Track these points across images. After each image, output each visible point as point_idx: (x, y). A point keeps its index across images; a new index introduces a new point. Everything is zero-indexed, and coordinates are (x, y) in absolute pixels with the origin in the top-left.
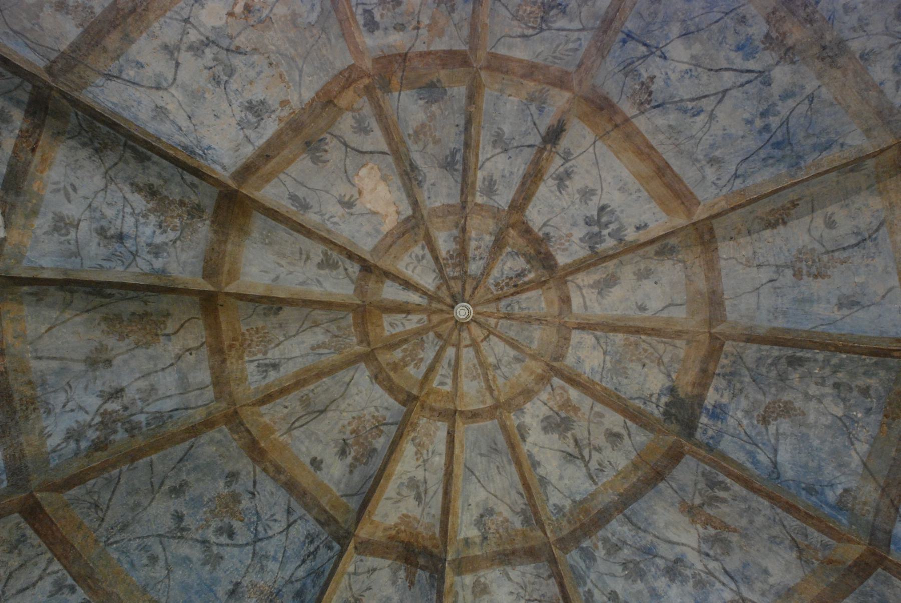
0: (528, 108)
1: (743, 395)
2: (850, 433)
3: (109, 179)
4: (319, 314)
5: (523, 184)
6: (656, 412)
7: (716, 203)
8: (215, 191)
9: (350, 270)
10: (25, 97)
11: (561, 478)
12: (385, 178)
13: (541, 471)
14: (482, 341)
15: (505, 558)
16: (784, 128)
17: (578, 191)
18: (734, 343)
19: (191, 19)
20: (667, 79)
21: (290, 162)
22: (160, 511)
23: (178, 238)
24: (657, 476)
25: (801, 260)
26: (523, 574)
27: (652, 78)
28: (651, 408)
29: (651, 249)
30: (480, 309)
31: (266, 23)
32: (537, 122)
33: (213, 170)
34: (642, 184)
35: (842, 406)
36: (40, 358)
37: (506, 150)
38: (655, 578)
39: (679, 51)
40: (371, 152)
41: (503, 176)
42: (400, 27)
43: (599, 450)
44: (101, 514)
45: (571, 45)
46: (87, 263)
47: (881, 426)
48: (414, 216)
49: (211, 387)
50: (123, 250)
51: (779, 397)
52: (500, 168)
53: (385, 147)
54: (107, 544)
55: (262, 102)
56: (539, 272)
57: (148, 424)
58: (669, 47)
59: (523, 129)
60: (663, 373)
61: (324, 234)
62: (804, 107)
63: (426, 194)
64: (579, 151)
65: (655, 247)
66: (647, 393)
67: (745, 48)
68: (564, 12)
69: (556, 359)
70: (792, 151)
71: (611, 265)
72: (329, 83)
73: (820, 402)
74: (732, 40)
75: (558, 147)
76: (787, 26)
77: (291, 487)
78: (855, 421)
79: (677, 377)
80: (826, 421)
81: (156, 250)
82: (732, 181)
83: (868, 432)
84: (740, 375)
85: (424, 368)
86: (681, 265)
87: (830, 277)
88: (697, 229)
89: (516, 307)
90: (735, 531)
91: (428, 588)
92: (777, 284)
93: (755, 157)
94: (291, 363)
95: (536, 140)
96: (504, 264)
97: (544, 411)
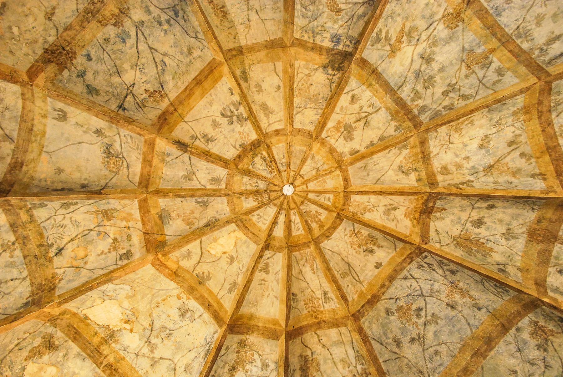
4: (295, 272)
5: (212, 162)
6: (338, 76)
8: (229, 336)
9: (269, 256)
11: (379, 128)
12: (215, 240)
13: (376, 140)
15: (426, 157)
16: (167, 11)
18: (295, 32)
20: (147, 82)
21: (211, 292)
24: (374, 72)
26: (435, 146)
27: (146, 91)
28: (336, 79)
30: (285, 182)
31: (134, 312)
33: (218, 339)
39: (129, 77)
40: (201, 249)
42: (129, 237)
43: (361, 108)
45: (129, 140)
52: (205, 174)
53: (198, 241)
61: (249, 273)
64: (191, 130)
69: (311, 136)
71: (254, 108)
72: (164, 275)
74: (119, 46)
76: (107, 13)
81: (265, 366)
82: (199, 40)
84: (313, 27)
85: (321, 210)
89: (283, 160)
90: (404, 25)
92: (259, 9)
93: (184, 27)
94: (323, 285)
95: (186, 156)
97: (341, 140)
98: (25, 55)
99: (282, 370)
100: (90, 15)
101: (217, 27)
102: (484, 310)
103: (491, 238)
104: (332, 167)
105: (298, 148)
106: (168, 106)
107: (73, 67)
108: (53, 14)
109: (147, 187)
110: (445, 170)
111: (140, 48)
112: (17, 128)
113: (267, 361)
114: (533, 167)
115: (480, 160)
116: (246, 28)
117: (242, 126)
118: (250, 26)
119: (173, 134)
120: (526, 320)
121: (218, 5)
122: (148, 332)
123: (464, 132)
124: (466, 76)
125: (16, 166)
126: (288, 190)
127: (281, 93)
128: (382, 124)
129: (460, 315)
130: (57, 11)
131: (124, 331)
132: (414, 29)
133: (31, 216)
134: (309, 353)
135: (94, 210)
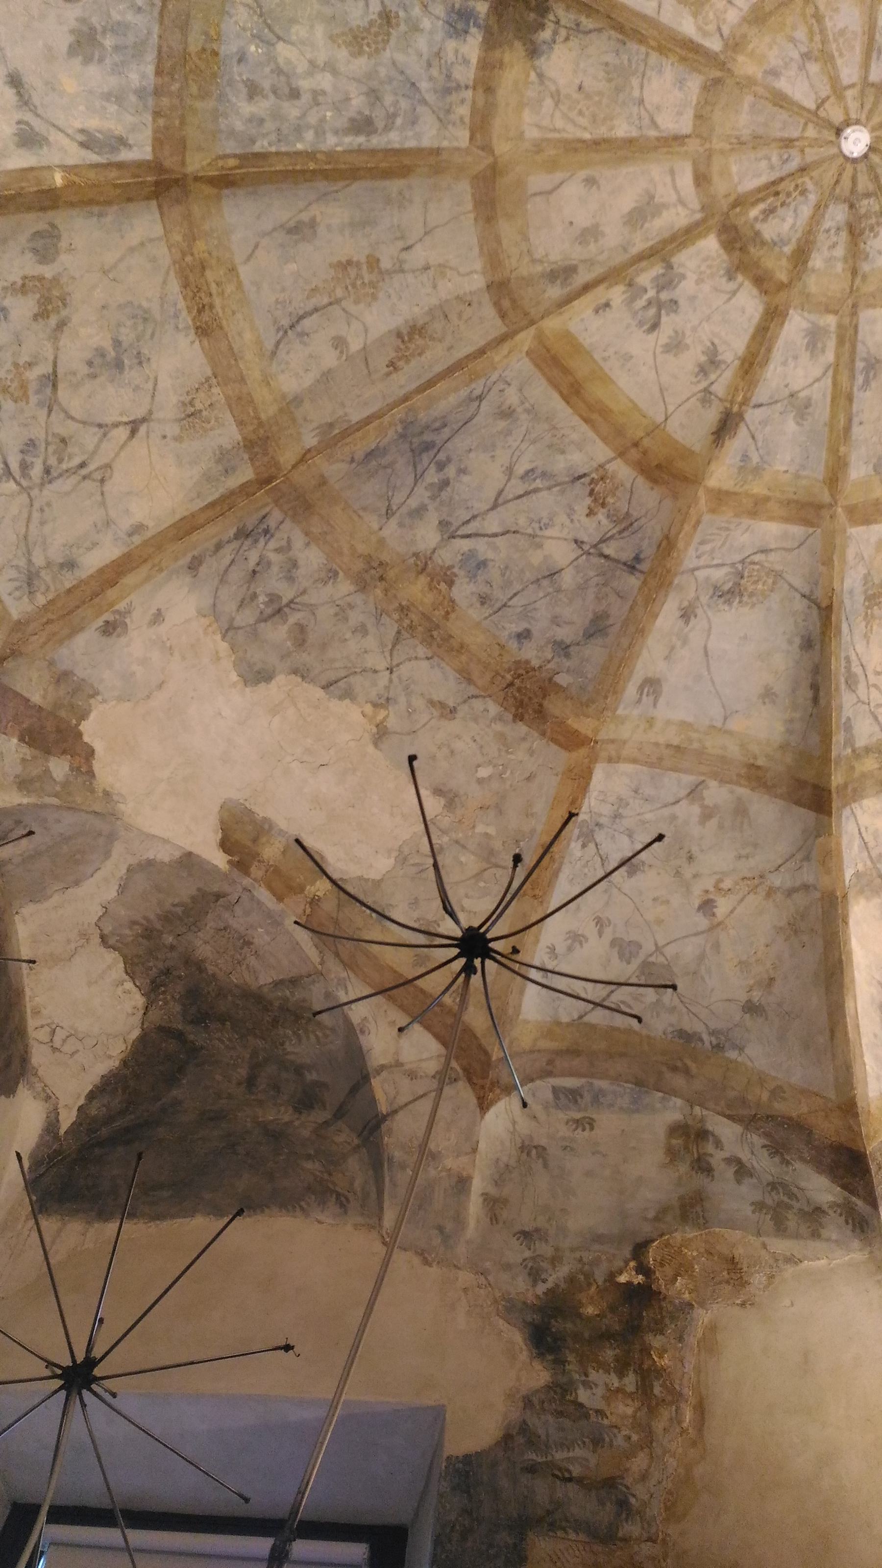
0: (761, 458)
1: (425, 57)
2: (261, 15)
5: (769, 350)
7: (506, 357)
14: (828, 98)
16: (420, 469)
17: (687, 347)
18: (456, 144)
20: (570, 512)
25: (373, 285)
27: (591, 513)
29: (583, 277)
30: (834, 150)
32: (751, 440)
34: (601, 369)
35: (281, 61)
39: (560, 552)
41: (796, 358)
45: (707, 547)
47: (219, 34)
51: (373, 61)
52: (797, 368)
56: (743, 219)
58: (573, 556)
59: (768, 428)
60: (550, 79)
62: (396, 500)
64: (687, 405)
66: (574, 43)
68: (716, 588)
69: (717, 82)
70: (411, 443)
71: (639, 245)
73: (312, 63)
74: (494, 573)
75: (721, 409)
76: (429, 598)
78: (258, 38)
79: (528, 76)
80: (299, 31)
82: (486, 389)
83: (236, 23)
84: (436, 92)
86: (537, 256)
87: (331, 265)
88: (526, 314)
89: (775, 159)
92: (400, 244)
93: (456, 427)
95: (752, 416)
96: (794, 225)
98: (531, 756)
100: (435, 633)
101: (450, 348)
104: (804, 15)
105: (743, 118)
106: (627, 462)
107: (549, 666)
108: (442, 705)
109: (819, 507)
111: (495, 528)
112: (675, 775)
118: (440, 265)
119: (697, 448)
121: (397, 350)
125: (755, 776)
126: (856, 141)
130: (436, 698)
133: (868, 750)
135: (864, 624)
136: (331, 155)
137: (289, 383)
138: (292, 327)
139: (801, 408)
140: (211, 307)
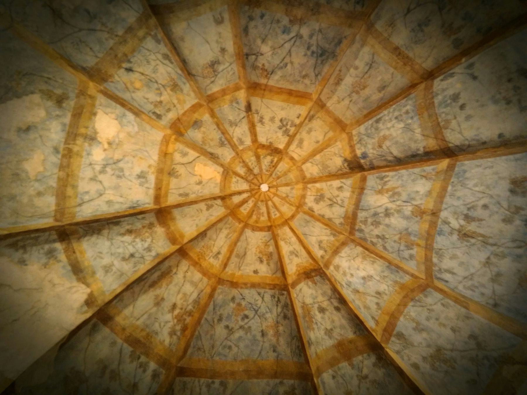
3: (110, 239)
4: (219, 225)
5: (251, 132)
6: (347, 171)
8: (153, 214)
9: (218, 203)
10: (55, 237)
11: (333, 214)
12: (205, 165)
13: (326, 217)
15: (336, 252)
17: (269, 121)
19: (92, 163)
20: (269, 62)
21: (168, 184)
22: (220, 331)
23: (152, 240)
24: (362, 189)
25: (355, 87)
26: (346, 252)
27: (263, 65)
28: (345, 170)
29: (307, 121)
31: (120, 144)
33: (146, 208)
36: (139, 319)
37: (236, 125)
38: (384, 221)
40: (194, 160)
41: (242, 135)
42: (169, 110)
43: (338, 196)
44: (202, 350)
45: (231, 73)
46: (129, 274)
48: (225, 170)
49: (204, 277)
50: (137, 259)
52: (240, 132)
53: (197, 155)
54: (212, 357)
55: (142, 172)
57: (194, 307)
61: (201, 199)
62: (320, 36)
63: (222, 160)
65: (307, 119)
66: (339, 167)
67: (286, 31)
69: (304, 179)
71: (298, 137)
72: (160, 148)
77: (254, 286)
78: (409, 124)
80: (399, 132)
81: (149, 249)
85: (266, 215)
89: (278, 173)
90: (398, 187)
91: (322, 281)
92: (353, 101)
93: (317, 65)
94: (223, 248)
95: (243, 114)
97: (312, 198)
99: (157, 261)
102: (275, 354)
103: (319, 324)
105: (292, 176)
110: (337, 268)
113: (153, 248)
114: (377, 314)
115: (356, 282)
116: (338, 101)
117: (283, 136)
120: (291, 382)
122: (111, 161)
123: (365, 262)
124: (395, 241)
127: (315, 146)
128: (336, 214)
129: (261, 343)
131: (101, 146)
132: (399, 194)
134: (174, 271)
136: (386, 109)
137: (366, 49)
138: (371, 65)
139: (232, 124)
140: (397, 56)
